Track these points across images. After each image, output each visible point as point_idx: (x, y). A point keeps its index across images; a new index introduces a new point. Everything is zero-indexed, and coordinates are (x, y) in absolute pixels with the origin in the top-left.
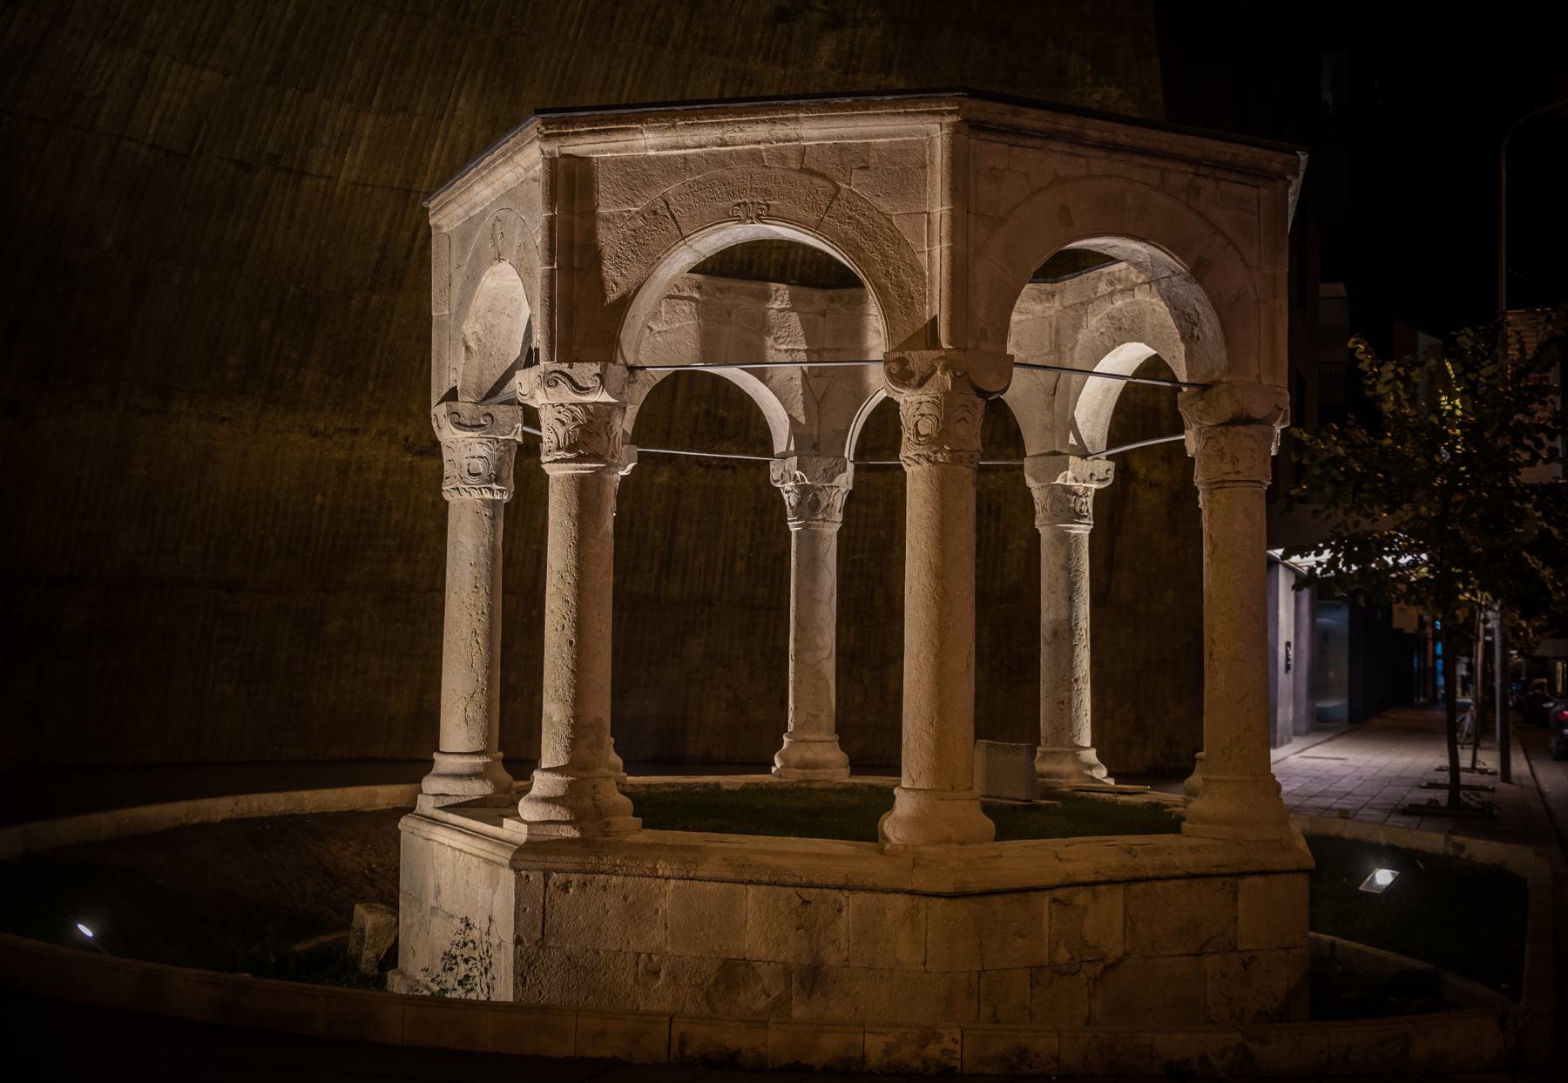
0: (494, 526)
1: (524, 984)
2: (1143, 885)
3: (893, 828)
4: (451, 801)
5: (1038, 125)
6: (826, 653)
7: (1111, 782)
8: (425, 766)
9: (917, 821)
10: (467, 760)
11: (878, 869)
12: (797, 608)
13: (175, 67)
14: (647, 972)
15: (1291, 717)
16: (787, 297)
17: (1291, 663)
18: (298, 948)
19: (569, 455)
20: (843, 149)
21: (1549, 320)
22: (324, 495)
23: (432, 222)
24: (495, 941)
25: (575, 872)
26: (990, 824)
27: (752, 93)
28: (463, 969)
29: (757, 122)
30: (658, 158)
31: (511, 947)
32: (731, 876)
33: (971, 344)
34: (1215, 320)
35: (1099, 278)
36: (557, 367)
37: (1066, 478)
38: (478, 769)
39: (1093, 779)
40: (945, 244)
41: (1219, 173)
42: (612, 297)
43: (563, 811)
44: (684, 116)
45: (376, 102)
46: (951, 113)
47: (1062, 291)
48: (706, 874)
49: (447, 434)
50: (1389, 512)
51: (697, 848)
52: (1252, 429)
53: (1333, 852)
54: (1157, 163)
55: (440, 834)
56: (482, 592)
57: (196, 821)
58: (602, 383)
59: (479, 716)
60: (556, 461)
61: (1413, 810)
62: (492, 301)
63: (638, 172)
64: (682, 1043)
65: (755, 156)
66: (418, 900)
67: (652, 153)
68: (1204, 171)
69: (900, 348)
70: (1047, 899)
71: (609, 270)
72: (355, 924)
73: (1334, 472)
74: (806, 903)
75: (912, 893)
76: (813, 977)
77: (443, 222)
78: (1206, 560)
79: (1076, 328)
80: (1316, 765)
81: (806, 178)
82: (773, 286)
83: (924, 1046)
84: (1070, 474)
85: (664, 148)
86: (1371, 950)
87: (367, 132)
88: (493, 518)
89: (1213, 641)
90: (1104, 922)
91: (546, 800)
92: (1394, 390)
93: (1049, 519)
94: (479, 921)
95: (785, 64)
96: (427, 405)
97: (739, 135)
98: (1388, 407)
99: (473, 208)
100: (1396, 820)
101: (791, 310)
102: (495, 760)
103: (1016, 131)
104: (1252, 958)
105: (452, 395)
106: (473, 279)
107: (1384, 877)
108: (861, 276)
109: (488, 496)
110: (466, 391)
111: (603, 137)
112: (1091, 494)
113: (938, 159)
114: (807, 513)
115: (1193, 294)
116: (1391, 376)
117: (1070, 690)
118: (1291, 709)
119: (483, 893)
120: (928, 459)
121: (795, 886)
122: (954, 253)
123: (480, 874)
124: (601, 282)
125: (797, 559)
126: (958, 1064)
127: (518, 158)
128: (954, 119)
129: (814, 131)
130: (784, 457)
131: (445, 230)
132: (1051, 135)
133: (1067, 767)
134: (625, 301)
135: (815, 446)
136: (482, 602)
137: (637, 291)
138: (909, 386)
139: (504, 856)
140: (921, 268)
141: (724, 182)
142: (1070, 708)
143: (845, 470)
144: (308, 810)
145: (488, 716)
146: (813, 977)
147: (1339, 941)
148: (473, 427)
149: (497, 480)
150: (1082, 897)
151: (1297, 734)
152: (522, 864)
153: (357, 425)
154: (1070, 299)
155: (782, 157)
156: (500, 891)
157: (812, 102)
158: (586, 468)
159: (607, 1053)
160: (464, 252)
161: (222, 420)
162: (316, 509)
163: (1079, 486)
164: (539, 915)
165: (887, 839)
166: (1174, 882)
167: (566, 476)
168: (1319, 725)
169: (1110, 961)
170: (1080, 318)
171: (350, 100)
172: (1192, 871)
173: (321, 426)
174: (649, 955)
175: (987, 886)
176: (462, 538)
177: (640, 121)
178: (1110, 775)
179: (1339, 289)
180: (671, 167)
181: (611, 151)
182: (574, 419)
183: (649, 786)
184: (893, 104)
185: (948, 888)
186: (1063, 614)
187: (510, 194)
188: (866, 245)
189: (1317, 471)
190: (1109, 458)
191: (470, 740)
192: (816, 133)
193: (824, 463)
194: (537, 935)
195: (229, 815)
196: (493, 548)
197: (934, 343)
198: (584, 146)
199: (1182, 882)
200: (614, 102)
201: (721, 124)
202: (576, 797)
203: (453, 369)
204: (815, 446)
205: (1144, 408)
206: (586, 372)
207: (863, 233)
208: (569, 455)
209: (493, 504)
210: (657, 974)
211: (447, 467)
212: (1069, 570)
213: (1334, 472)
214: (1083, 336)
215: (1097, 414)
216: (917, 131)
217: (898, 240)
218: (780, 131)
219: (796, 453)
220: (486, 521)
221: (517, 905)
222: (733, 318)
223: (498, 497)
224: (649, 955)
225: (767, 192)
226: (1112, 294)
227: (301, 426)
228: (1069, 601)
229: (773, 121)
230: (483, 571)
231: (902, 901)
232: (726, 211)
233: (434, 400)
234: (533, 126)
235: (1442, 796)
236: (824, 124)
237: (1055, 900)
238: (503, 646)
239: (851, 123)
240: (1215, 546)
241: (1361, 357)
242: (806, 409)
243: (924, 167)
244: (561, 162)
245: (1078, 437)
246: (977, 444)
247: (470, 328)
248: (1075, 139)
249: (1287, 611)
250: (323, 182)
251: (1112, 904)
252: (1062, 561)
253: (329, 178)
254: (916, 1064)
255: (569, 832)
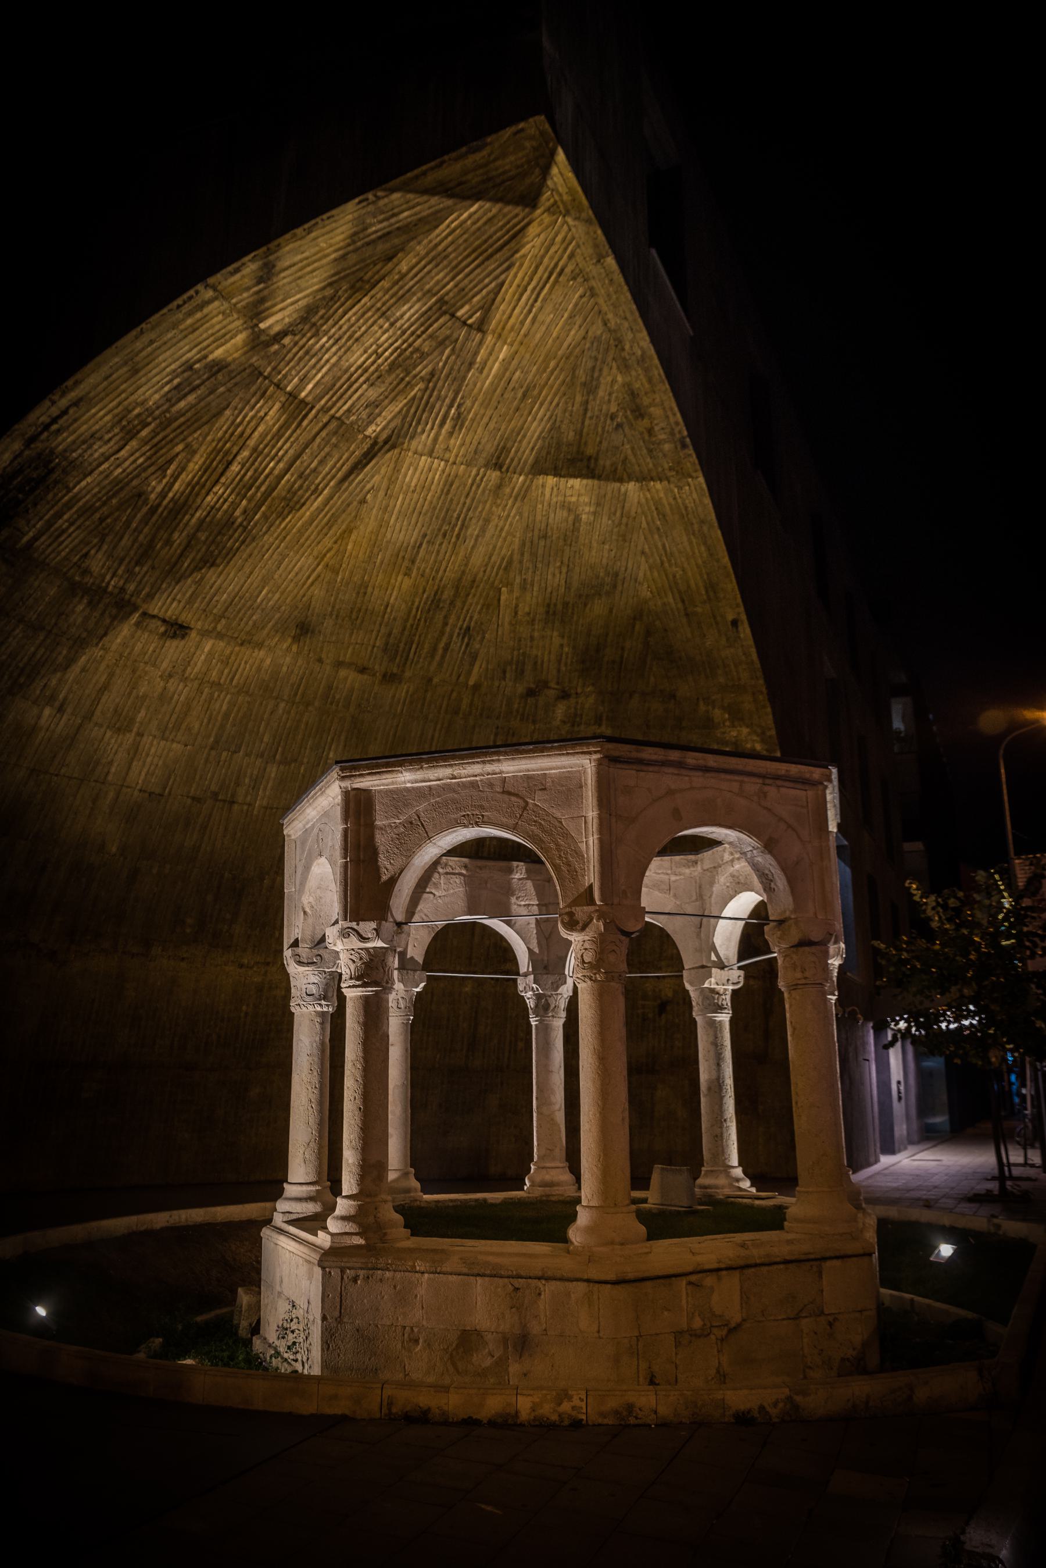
0: (323, 1029)
1: (328, 1349)
2: (753, 1270)
3: (575, 1235)
4: (294, 1217)
5: (654, 757)
6: (557, 1107)
7: (754, 1190)
8: (276, 1193)
9: (590, 1230)
10: (305, 1188)
11: (566, 1265)
12: (537, 1076)
13: (155, 743)
14: (410, 1340)
15: (905, 1132)
16: (524, 871)
17: (903, 1095)
18: (199, 1319)
19: (358, 983)
20: (529, 778)
21: (1031, 864)
22: (248, 1005)
23: (285, 833)
24: (311, 1318)
25: (362, 1269)
26: (643, 1229)
27: (515, 740)
28: (291, 1337)
29: (474, 763)
30: (413, 788)
31: (320, 1322)
32: (465, 1270)
33: (616, 901)
34: (783, 878)
35: (724, 851)
36: (350, 924)
37: (710, 983)
38: (312, 1194)
39: (740, 1189)
40: (596, 836)
41: (779, 783)
42: (384, 878)
43: (354, 1226)
44: (428, 761)
45: (278, 757)
46: (596, 752)
47: (702, 860)
48: (449, 1270)
49: (293, 969)
50: (942, 994)
51: (443, 1251)
52: (813, 949)
53: (901, 1237)
54: (736, 778)
55: (284, 1242)
56: (315, 1073)
57: (142, 1229)
58: (378, 934)
59: (313, 1158)
60: (350, 987)
61: (977, 1199)
62: (316, 884)
63: (400, 798)
64: (390, 1404)
65: (473, 785)
66: (271, 1287)
67: (409, 785)
68: (768, 781)
69: (569, 906)
70: (684, 1282)
71: (383, 861)
72: (238, 1303)
73: (904, 969)
74: (517, 1289)
75: (588, 1281)
76: (522, 1343)
77: (291, 832)
78: (789, 1038)
79: (712, 883)
80: (915, 1164)
81: (506, 797)
82: (515, 864)
83: (560, 1404)
84: (713, 980)
85: (416, 782)
86: (938, 1305)
87: (273, 775)
88: (322, 1024)
89: (797, 1094)
90: (726, 1298)
91: (343, 1218)
92: (938, 913)
93: (701, 1011)
94: (302, 1303)
95: (534, 722)
96: (282, 951)
97: (463, 772)
98: (935, 925)
99: (307, 823)
100: (966, 1207)
101: (526, 879)
102: (324, 1188)
103: (641, 762)
104: (835, 1319)
105: (296, 944)
106: (307, 868)
107: (946, 1250)
108: (543, 859)
109: (319, 1009)
110: (304, 941)
111: (377, 777)
112: (729, 993)
113: (589, 781)
114: (542, 1012)
115: (766, 861)
116: (934, 904)
117: (721, 1127)
118: (905, 1127)
119: (305, 1283)
120: (591, 980)
121: (508, 1277)
122: (601, 841)
123: (303, 1269)
124: (377, 869)
125: (537, 1044)
126: (584, 1417)
127: (328, 791)
128: (598, 756)
129: (511, 767)
130: (526, 975)
131: (293, 837)
132: (664, 763)
133: (722, 1181)
134: (393, 881)
135: (546, 968)
136: (315, 1080)
137: (400, 874)
138: (576, 930)
139: (315, 1257)
140: (581, 852)
141: (454, 801)
142: (722, 1140)
143: (565, 983)
144: (219, 1219)
145: (319, 1157)
146: (522, 1343)
147: (917, 1298)
148: (308, 964)
149: (325, 999)
150: (709, 1280)
151: (912, 1142)
152: (326, 1264)
153: (269, 960)
154: (707, 865)
155: (491, 785)
156: (314, 1282)
157: (508, 749)
158: (369, 991)
159: (338, 1411)
160: (303, 852)
161: (183, 959)
162: (242, 1015)
163: (720, 988)
164: (338, 1300)
165: (572, 1243)
166: (775, 1267)
167: (356, 997)
168: (928, 1136)
169: (733, 1325)
170: (713, 877)
171: (262, 756)
172: (788, 1258)
173: (246, 961)
174: (412, 1328)
175: (641, 1275)
176: (302, 1037)
177: (401, 766)
178: (752, 1186)
179: (919, 846)
180: (421, 794)
181: (383, 785)
182: (361, 959)
183: (438, 1202)
184: (560, 748)
185: (611, 1277)
186: (714, 1076)
187: (326, 814)
188: (546, 838)
189: (892, 969)
190: (739, 968)
191: (307, 1174)
192: (511, 768)
193: (551, 979)
194: (337, 1314)
195: (167, 1224)
196: (323, 1043)
197: (592, 902)
198: (367, 782)
199: (782, 1266)
200: (491, 744)
201: (451, 766)
202: (364, 1218)
203: (295, 927)
204: (546, 968)
205: (753, 938)
206: (368, 927)
207: (544, 831)
208: (358, 983)
209: (322, 1014)
210: (417, 1341)
211: (293, 990)
212: (716, 1045)
213: (904, 969)
214: (716, 888)
215: (729, 939)
216: (576, 765)
217: (566, 835)
218: (489, 768)
219: (533, 972)
220: (318, 1026)
221: (323, 1293)
222: (489, 885)
223: (325, 1009)
224: (412, 1328)
225: (482, 807)
226: (732, 861)
227: (233, 962)
228: (717, 1064)
229: (484, 762)
230: (316, 1059)
231: (582, 1287)
232: (456, 820)
233: (285, 946)
234: (335, 772)
235: (994, 1186)
236: (516, 762)
237: (690, 1283)
238: (330, 1111)
239: (533, 761)
240: (794, 1029)
241: (915, 892)
242: (539, 943)
243: (581, 787)
244: (352, 793)
245: (717, 955)
246: (624, 967)
247: (307, 900)
248: (680, 765)
249: (896, 1059)
250: (245, 807)
251: (732, 1283)
252: (711, 1039)
253: (250, 805)
254: (554, 1417)
255: (359, 1241)
